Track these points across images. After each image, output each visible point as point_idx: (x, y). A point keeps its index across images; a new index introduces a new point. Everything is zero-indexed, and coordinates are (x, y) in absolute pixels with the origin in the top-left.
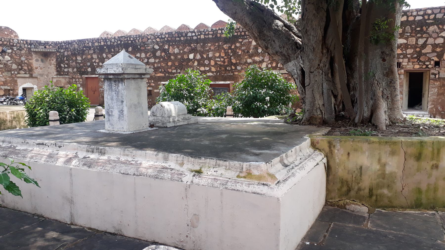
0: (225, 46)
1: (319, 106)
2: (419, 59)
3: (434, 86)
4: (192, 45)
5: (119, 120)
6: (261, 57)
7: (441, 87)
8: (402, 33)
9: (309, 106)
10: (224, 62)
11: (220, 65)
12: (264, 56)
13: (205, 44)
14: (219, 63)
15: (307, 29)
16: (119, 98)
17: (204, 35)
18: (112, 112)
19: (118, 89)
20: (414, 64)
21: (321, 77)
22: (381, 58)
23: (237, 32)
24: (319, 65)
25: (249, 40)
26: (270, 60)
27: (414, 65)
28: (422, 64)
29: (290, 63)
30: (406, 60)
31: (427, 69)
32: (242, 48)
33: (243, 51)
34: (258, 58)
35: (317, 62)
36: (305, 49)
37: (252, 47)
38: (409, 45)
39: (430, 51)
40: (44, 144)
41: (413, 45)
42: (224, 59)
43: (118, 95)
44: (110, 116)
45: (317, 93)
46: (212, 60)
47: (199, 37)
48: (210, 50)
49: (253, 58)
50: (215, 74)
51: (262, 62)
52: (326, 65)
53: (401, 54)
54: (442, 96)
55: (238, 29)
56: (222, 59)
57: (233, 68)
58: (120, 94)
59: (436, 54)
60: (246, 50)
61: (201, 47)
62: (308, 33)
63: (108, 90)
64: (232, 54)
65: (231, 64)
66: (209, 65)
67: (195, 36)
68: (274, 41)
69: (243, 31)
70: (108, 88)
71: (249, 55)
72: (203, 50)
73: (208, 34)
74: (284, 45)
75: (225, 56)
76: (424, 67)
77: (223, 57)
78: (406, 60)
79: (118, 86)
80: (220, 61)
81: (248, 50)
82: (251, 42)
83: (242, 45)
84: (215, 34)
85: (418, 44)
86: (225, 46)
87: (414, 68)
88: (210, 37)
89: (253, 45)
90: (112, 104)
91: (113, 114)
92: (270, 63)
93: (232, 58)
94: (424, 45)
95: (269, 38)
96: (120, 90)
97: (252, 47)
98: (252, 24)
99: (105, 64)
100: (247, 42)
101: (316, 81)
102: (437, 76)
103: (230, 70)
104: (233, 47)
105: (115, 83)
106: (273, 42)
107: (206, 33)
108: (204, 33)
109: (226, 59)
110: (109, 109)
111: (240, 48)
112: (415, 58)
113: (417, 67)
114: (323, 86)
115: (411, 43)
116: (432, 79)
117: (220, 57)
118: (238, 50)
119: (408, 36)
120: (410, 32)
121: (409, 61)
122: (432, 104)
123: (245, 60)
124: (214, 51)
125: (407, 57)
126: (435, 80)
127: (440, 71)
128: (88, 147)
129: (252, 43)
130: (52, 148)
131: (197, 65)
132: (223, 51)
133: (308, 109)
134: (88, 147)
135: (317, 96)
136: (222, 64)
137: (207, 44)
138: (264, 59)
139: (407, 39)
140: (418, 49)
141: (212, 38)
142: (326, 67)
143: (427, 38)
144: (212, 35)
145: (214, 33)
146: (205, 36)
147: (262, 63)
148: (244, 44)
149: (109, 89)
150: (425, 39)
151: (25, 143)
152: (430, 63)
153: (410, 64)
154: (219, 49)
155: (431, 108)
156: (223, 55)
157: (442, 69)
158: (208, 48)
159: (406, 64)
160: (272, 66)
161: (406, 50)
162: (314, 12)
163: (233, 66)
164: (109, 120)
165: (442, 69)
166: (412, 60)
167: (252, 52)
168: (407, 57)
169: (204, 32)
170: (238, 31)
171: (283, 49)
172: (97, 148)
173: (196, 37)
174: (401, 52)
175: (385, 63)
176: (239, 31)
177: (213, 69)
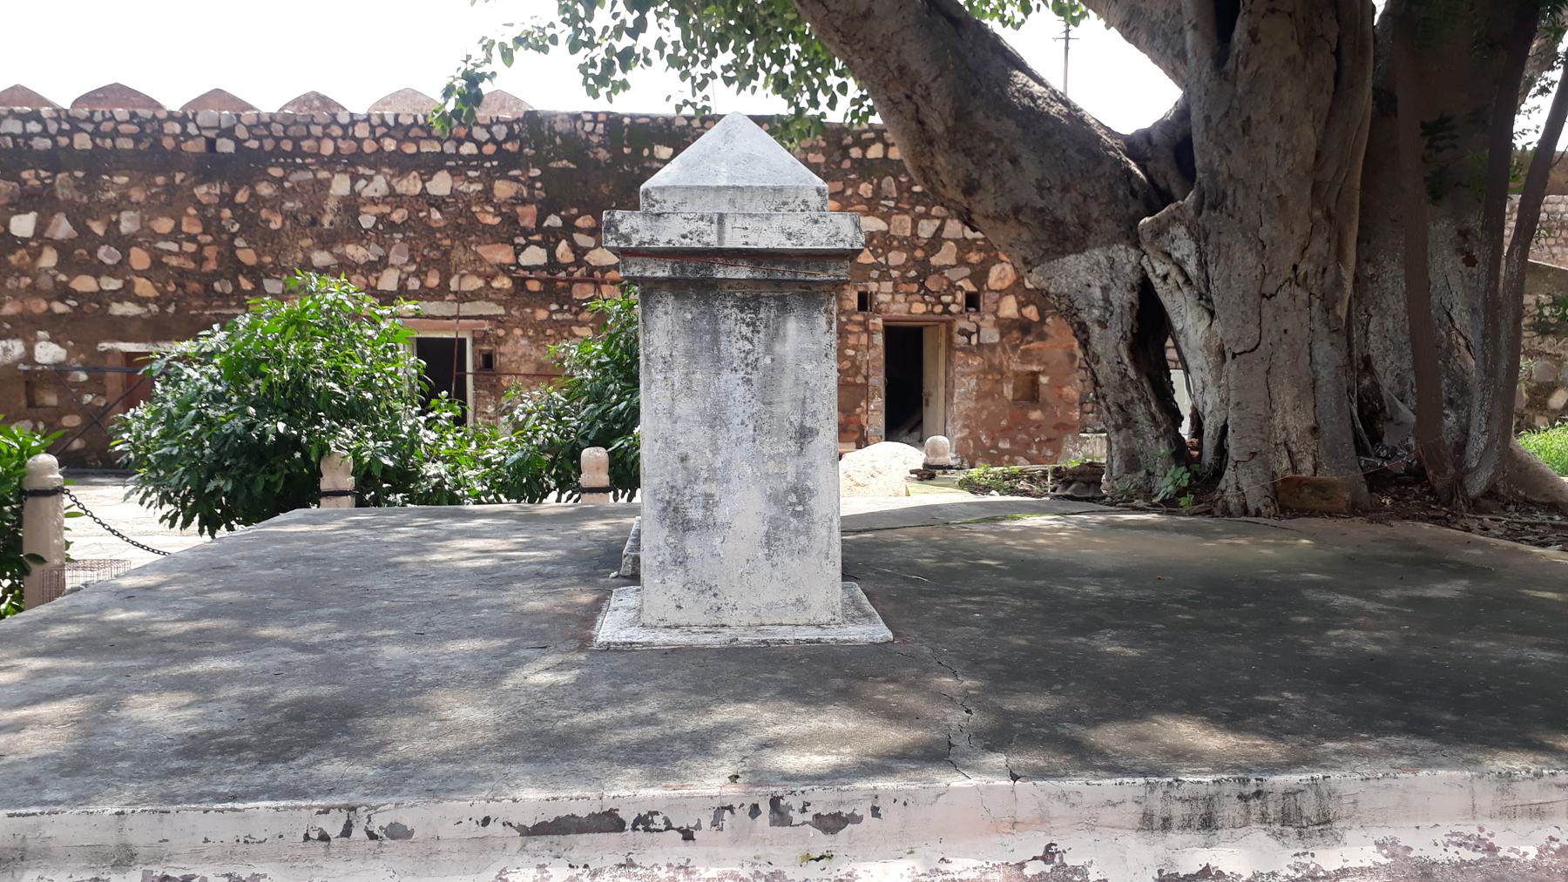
0: (201, 191)
1: (1284, 435)
2: (922, 285)
3: (967, 370)
4: (25, 175)
5: (769, 557)
6: (373, 246)
7: (985, 372)
8: (871, 198)
9: (1258, 434)
10: (198, 257)
11: (181, 272)
12: (386, 245)
13: (98, 176)
14: (174, 261)
15: (1249, 118)
16: (777, 410)
17: (93, 135)
18: (709, 502)
19: (769, 350)
20: (911, 298)
21: (1305, 318)
22: (1460, 250)
23: (259, 138)
24: (1295, 267)
25: (315, 175)
26: (412, 260)
27: (911, 303)
28: (933, 300)
29: (1072, 257)
30: (887, 286)
31: (947, 317)
32: (283, 203)
33: (293, 216)
34: (362, 251)
35: (1291, 254)
36: (1230, 199)
37: (331, 204)
38: (895, 238)
39: (951, 260)
40: (628, 816)
41: (906, 238)
42: (201, 246)
43: (767, 390)
44: (692, 535)
45: (1285, 381)
46: (140, 245)
47: (63, 141)
48: (124, 203)
49: (337, 250)
50: (154, 308)
51: (382, 264)
52: (1325, 270)
53: (872, 266)
54: (988, 401)
55: (263, 124)
56: (190, 247)
57: (246, 285)
58: (787, 382)
59: (967, 271)
60: (306, 213)
61: (78, 187)
62: (1252, 132)
63: (681, 360)
64: (237, 226)
65: (234, 268)
66: (121, 268)
67: (45, 133)
68: (1014, 161)
69: (287, 137)
70: (681, 344)
71: (319, 236)
72: (85, 199)
73: (115, 134)
74: (1068, 179)
75: (204, 233)
76: (939, 309)
77: (192, 238)
78: (887, 286)
79: (775, 335)
80: (176, 254)
81: (315, 214)
82: (325, 185)
83: (285, 194)
84: (147, 136)
85: (918, 238)
86: (204, 189)
87: (909, 312)
88: (126, 146)
89: (336, 197)
90: (716, 451)
91: (722, 514)
92: (416, 274)
93: (239, 242)
94: (936, 242)
95: (992, 146)
96: (790, 359)
97: (331, 204)
98: (932, 77)
99: (662, 189)
100: (307, 181)
101: (1285, 331)
102: (974, 340)
103: (232, 294)
104: (242, 197)
105: (748, 317)
106: (1007, 165)
107: (102, 128)
108: (89, 127)
109: (209, 245)
110: (680, 483)
111: (274, 204)
112: (914, 280)
113: (919, 308)
114: (1315, 353)
115: (899, 233)
116: (962, 349)
117: (176, 235)
118: (264, 213)
119: (889, 208)
120: (895, 195)
121: (896, 291)
122: (964, 426)
123: (300, 255)
124: (150, 209)
125: (890, 278)
126: (969, 351)
127: (981, 324)
128: (1159, 793)
129: (329, 187)
130: (735, 841)
131: (55, 268)
132: (192, 211)
133: (1254, 450)
134: (1159, 793)
135: (1286, 396)
136: (191, 265)
137: (106, 177)
138: (387, 257)
139: (886, 217)
140: (919, 254)
141: (135, 152)
142: (1327, 274)
143: (944, 220)
144: (137, 138)
145: (142, 130)
146: (98, 141)
147: (378, 271)
148: (293, 188)
149: (691, 355)
150: (938, 223)
151: (358, 833)
152: (955, 298)
153: (900, 298)
154: (173, 200)
155: (963, 439)
156: (191, 226)
157: (987, 317)
158: (112, 194)
159: (889, 298)
160: (422, 286)
161: (885, 254)
162: (1294, 49)
163: (245, 276)
164: (681, 561)
165: (987, 317)
166: (904, 287)
167: (331, 224)
168: (890, 278)
169: (93, 122)
170: (265, 132)
171: (1062, 199)
172: (1251, 789)
173: (48, 143)
174: (871, 260)
175: (1475, 270)
176: (271, 135)
177: (144, 287)
